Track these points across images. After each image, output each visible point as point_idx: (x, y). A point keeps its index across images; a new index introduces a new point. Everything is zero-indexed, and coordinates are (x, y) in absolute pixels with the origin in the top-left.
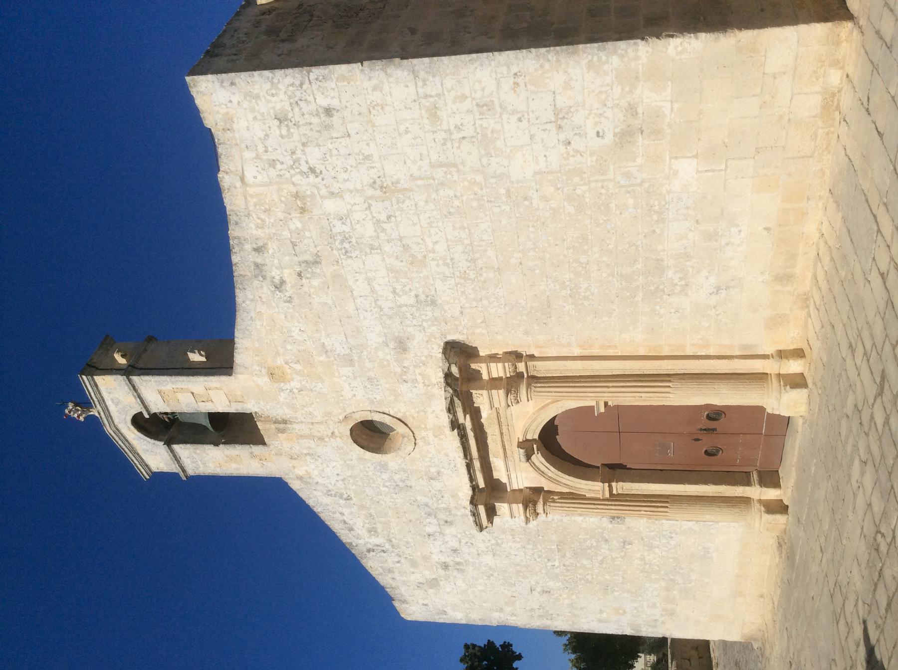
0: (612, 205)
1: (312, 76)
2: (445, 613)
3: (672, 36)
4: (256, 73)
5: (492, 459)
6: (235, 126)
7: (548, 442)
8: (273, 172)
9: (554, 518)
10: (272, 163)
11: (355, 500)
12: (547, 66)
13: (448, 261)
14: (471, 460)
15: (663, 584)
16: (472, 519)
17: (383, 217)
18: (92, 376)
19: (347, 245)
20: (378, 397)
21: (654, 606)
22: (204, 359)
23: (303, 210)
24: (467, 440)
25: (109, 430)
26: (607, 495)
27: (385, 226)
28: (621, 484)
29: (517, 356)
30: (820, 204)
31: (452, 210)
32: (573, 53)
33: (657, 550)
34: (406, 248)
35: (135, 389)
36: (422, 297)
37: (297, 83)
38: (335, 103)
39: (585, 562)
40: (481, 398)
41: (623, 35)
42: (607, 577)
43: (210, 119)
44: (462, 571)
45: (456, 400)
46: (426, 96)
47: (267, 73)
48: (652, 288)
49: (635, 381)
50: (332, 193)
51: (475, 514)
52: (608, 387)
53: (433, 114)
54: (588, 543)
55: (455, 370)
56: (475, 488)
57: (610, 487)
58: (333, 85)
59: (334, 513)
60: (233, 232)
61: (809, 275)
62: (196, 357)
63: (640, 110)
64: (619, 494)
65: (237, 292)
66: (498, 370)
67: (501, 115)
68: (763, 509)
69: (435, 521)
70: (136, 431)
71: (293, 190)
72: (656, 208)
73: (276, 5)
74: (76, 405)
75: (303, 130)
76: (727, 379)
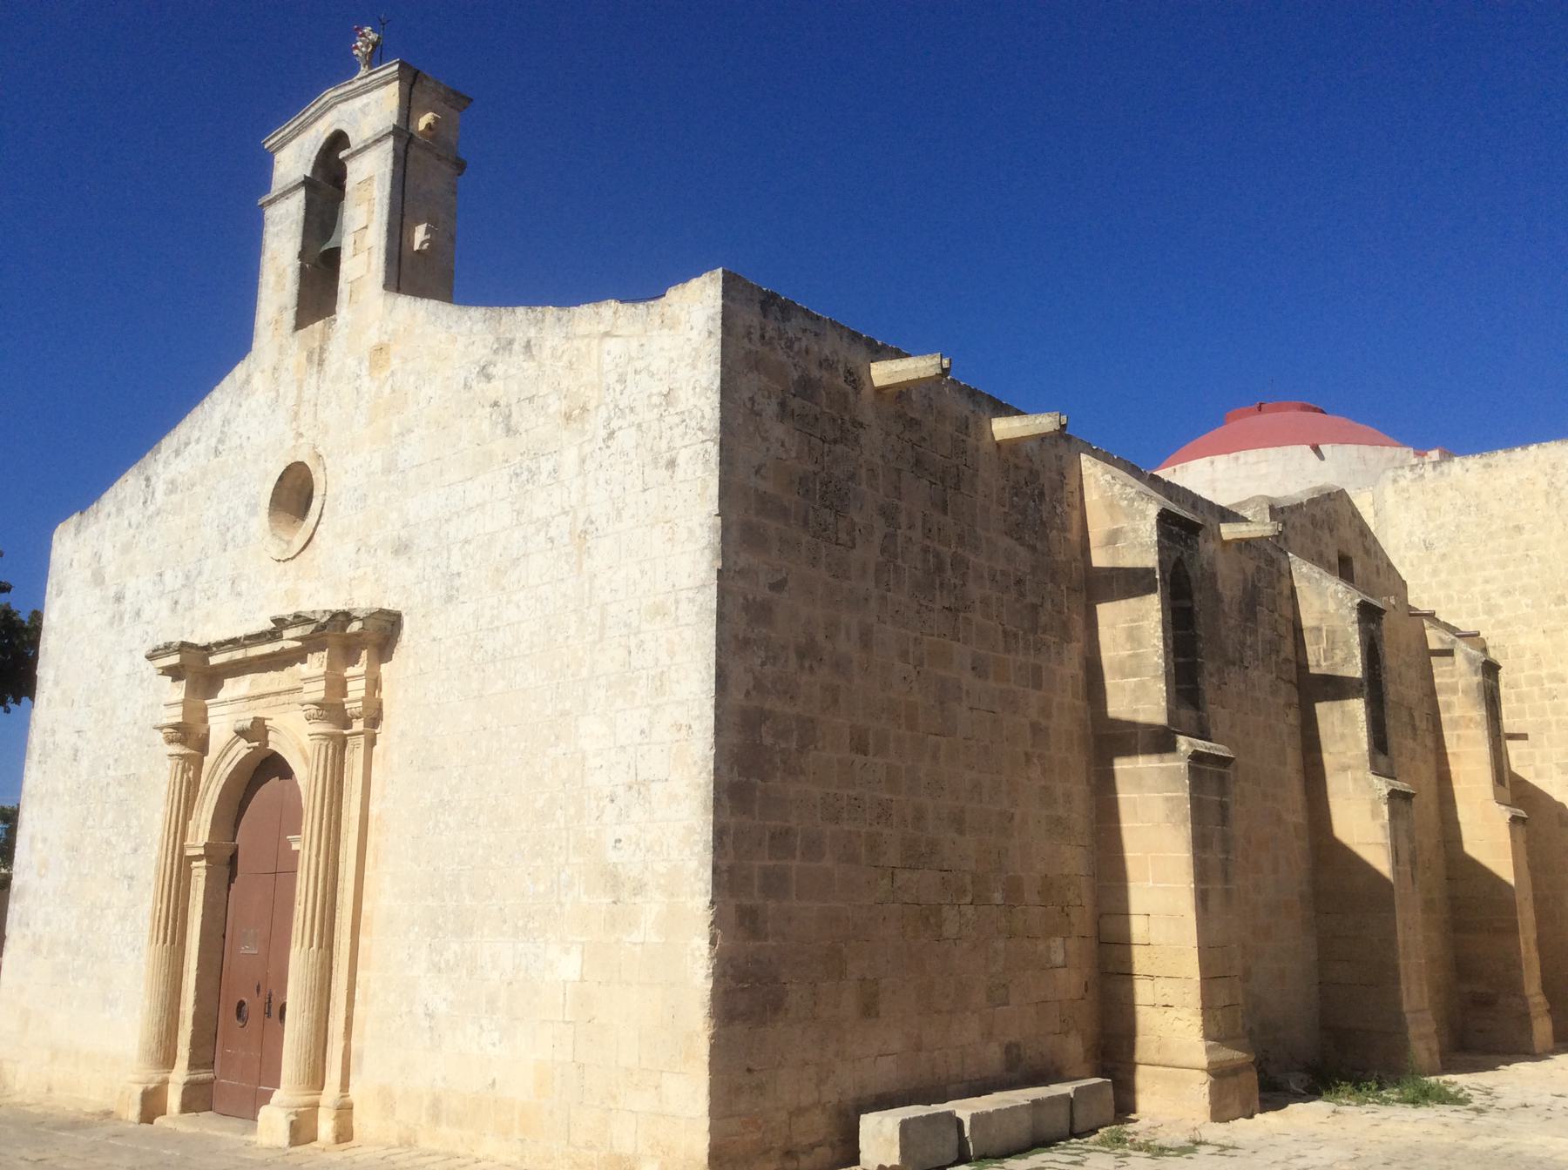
0: (539, 862)
1: (710, 445)
2: (59, 594)
3: (713, 942)
4: (718, 367)
5: (249, 677)
6: (666, 331)
7: (266, 767)
8: (613, 377)
9: (160, 766)
10: (622, 380)
11: (214, 461)
12: (695, 771)
13: (496, 623)
14: (245, 646)
15: (74, 937)
16: (161, 643)
17: (553, 532)
18: (400, 79)
19: (525, 476)
20: (341, 508)
21: (47, 923)
22: (416, 247)
23: (568, 417)
24: (270, 641)
25: (330, 94)
26: (189, 853)
27: (543, 534)
28: (203, 873)
29: (374, 719)
30: (515, 1158)
31: (553, 631)
32: (705, 807)
33: (118, 927)
34: (515, 562)
35: (378, 141)
36: (457, 582)
37: (705, 424)
38: (680, 474)
39: (110, 817)
40: (316, 664)
41: (725, 876)
42: (90, 850)
43: (674, 295)
44: (112, 624)
45: (312, 627)
46: (677, 602)
47: (718, 382)
48: (440, 920)
49: (324, 896)
50: (584, 462)
51: (167, 649)
52: (318, 855)
53: (659, 611)
54: (134, 822)
55: (355, 627)
56: (208, 649)
57: (198, 858)
58: (699, 474)
59: (200, 429)
60: (551, 311)
61: (436, 1147)
62: (420, 235)
63: (638, 899)
64: (191, 870)
65: (482, 310)
66: (356, 689)
67: (649, 705)
68: (152, 1086)
69: (178, 586)
70: (327, 135)
71: (591, 406)
72: (530, 925)
73: (866, 391)
74: (375, 45)
75: (655, 425)
76: (318, 1030)
